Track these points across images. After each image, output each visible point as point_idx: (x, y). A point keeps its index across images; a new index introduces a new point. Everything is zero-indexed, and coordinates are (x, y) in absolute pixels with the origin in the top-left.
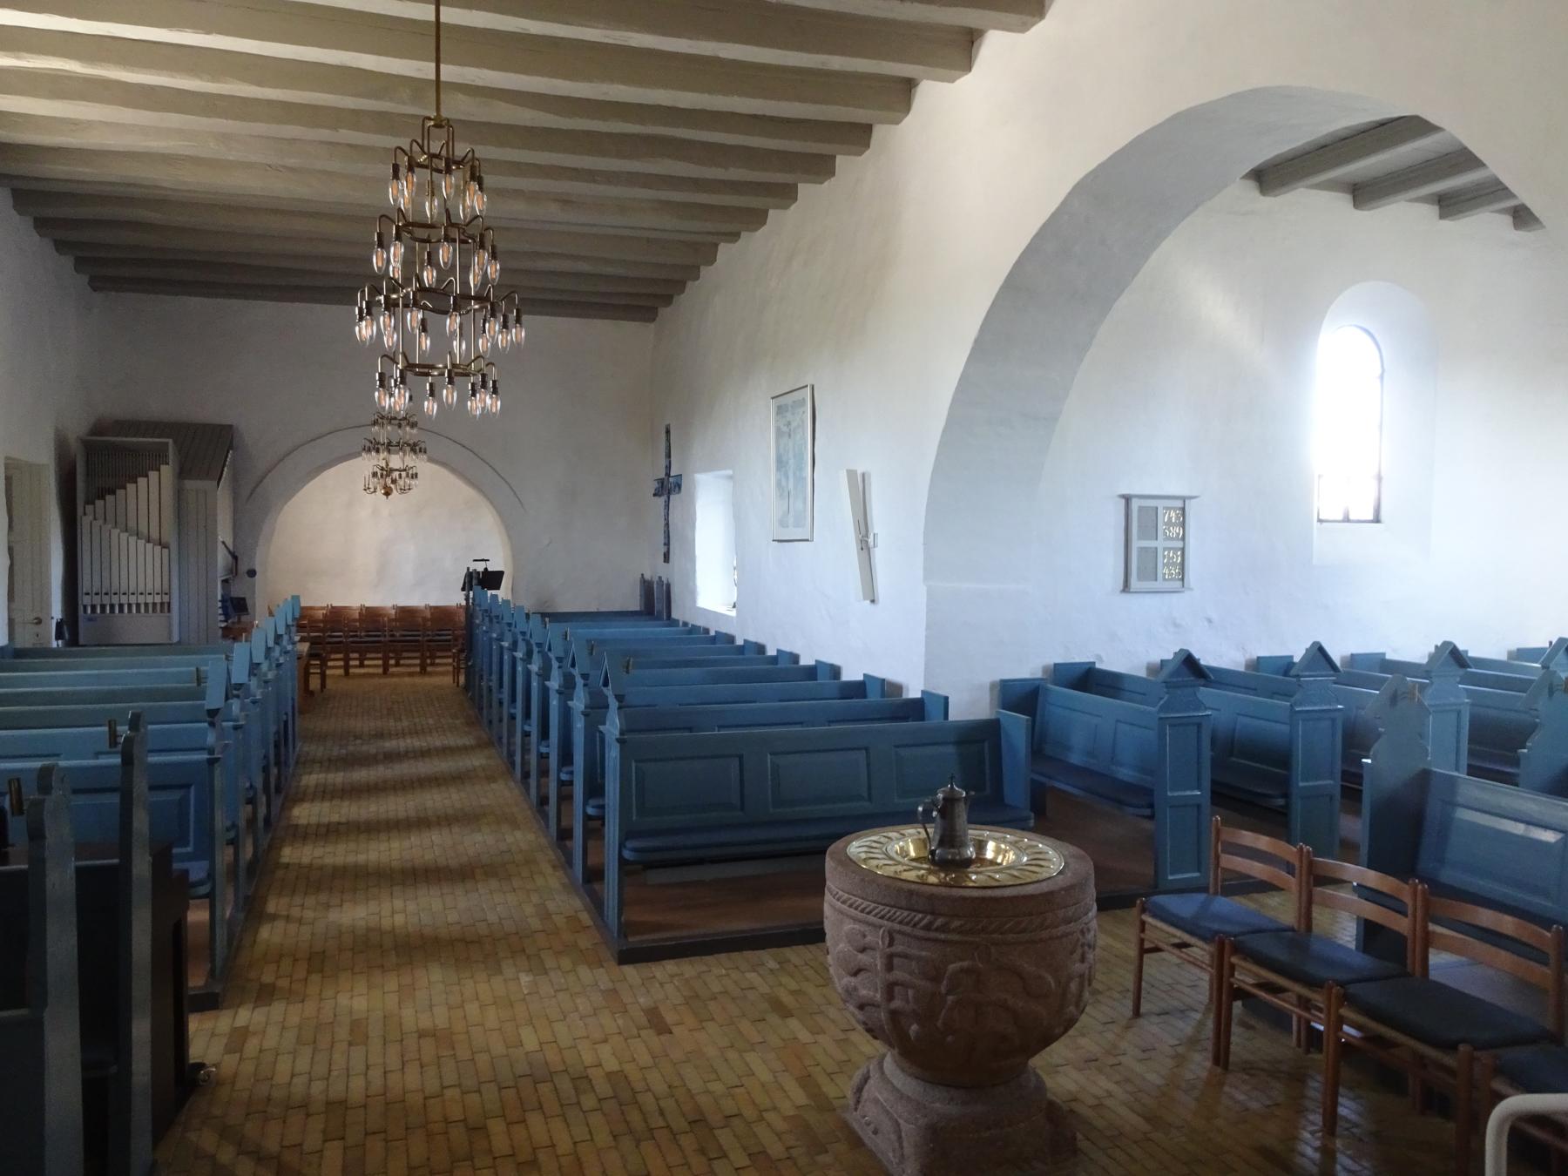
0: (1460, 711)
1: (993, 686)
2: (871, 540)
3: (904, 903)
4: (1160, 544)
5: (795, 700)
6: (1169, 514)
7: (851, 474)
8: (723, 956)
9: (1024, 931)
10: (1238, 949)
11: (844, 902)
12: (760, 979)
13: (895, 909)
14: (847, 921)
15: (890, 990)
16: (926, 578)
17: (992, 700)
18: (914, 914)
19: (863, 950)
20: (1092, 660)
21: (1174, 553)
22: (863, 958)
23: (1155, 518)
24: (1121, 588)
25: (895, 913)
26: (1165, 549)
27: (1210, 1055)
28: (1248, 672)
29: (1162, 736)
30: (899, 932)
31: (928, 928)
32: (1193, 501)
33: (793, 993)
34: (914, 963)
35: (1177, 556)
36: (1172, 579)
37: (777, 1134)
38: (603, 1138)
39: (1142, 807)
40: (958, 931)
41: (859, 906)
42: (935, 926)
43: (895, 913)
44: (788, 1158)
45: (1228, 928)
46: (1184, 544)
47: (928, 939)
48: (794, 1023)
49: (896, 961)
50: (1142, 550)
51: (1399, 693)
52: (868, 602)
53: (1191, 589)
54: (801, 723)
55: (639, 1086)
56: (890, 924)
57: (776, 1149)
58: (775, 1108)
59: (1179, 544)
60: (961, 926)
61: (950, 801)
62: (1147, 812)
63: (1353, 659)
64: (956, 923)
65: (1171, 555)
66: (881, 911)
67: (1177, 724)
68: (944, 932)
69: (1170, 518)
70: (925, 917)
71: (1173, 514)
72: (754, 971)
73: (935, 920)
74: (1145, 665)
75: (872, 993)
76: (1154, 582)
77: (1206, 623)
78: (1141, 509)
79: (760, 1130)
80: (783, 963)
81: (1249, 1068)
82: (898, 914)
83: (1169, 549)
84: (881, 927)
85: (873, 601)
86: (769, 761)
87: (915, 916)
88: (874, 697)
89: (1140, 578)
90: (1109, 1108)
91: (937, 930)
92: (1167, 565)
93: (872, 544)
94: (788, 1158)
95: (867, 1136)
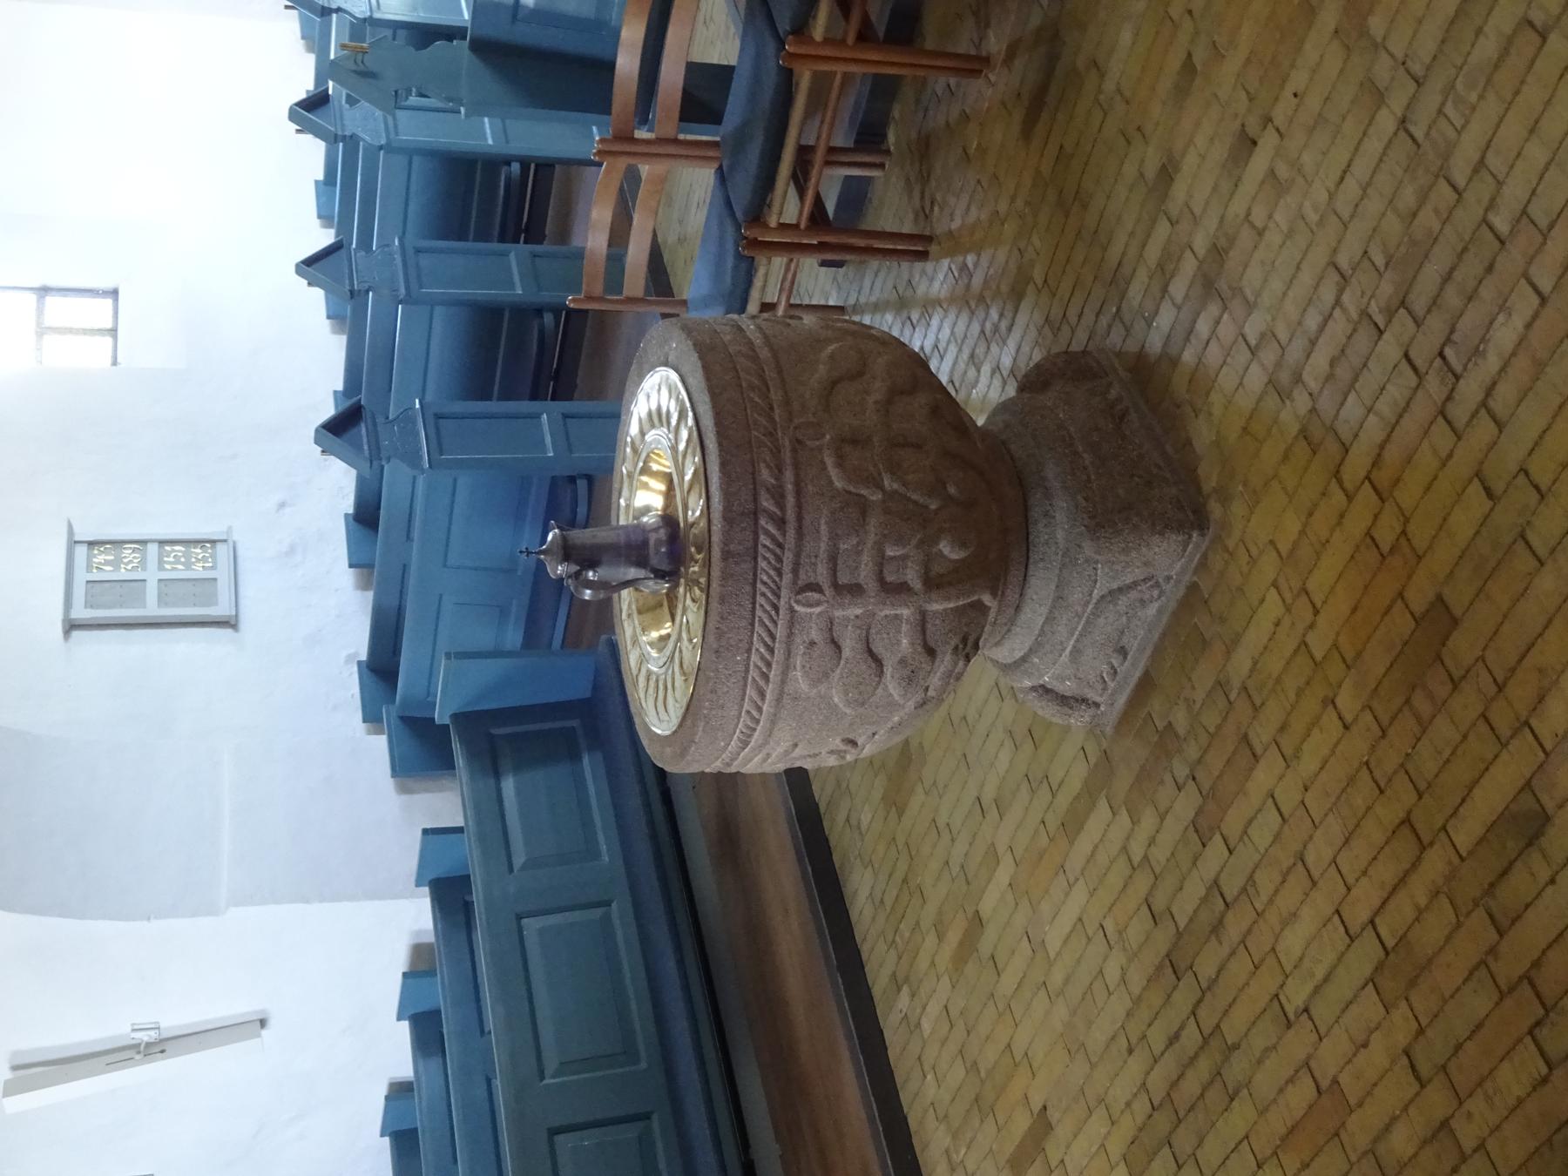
0: (435, 415)
1: (403, 789)
2: (145, 1037)
3: (746, 566)
4: (152, 576)
5: (453, 1135)
6: (100, 563)
7: (11, 1089)
8: (905, 1098)
9: (762, 378)
10: (756, 216)
11: (762, 695)
12: (928, 1009)
13: (759, 585)
14: (789, 688)
15: (894, 590)
16: (212, 910)
17: (426, 791)
18: (761, 550)
19: (837, 646)
20: (355, 668)
21: (168, 556)
22: (850, 644)
23: (107, 585)
24: (229, 631)
25: (765, 583)
26: (161, 567)
27: (918, 265)
28: (374, 584)
29: (459, 464)
30: (795, 572)
31: (781, 523)
32: (76, 529)
33: (940, 937)
34: (843, 547)
35: (174, 551)
36: (213, 556)
37: (1162, 819)
38: (1240, 1117)
39: (575, 492)
40: (779, 470)
41: (762, 658)
42: (773, 508)
43: (765, 583)
44: (1194, 779)
45: (730, 246)
46: (153, 541)
47: (800, 519)
48: (987, 907)
49: (843, 579)
50: (162, 600)
51: (354, 67)
52: (264, 1032)
53: (230, 528)
54: (489, 1082)
55: (1141, 1107)
56: (784, 593)
57: (1185, 806)
58: (1125, 849)
59: (153, 549)
60: (768, 466)
61: (567, 552)
62: (582, 485)
63: (325, 217)
64: (765, 475)
65: (171, 559)
66: (765, 611)
67: (437, 446)
68: (783, 496)
69: (107, 563)
70: (763, 528)
71: (101, 558)
72: (918, 1025)
73: (765, 510)
74: (359, 593)
75: (905, 628)
76: (219, 582)
77: (287, 510)
78: (89, 604)
79: (1160, 855)
80: (897, 983)
81: (924, 214)
82: (765, 578)
83: (161, 563)
84: (792, 611)
85: (263, 1023)
86: (552, 1081)
87: (765, 546)
88: (438, 995)
89: (211, 600)
90: (1015, 360)
91: (782, 507)
92: (188, 566)
93: (152, 1033)
94: (1194, 779)
95: (1132, 671)
